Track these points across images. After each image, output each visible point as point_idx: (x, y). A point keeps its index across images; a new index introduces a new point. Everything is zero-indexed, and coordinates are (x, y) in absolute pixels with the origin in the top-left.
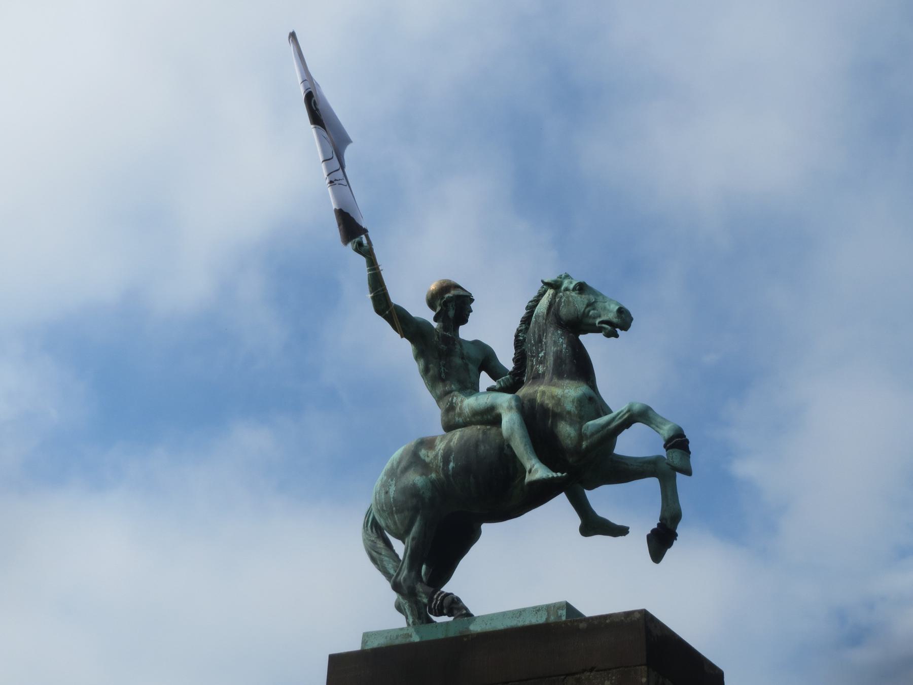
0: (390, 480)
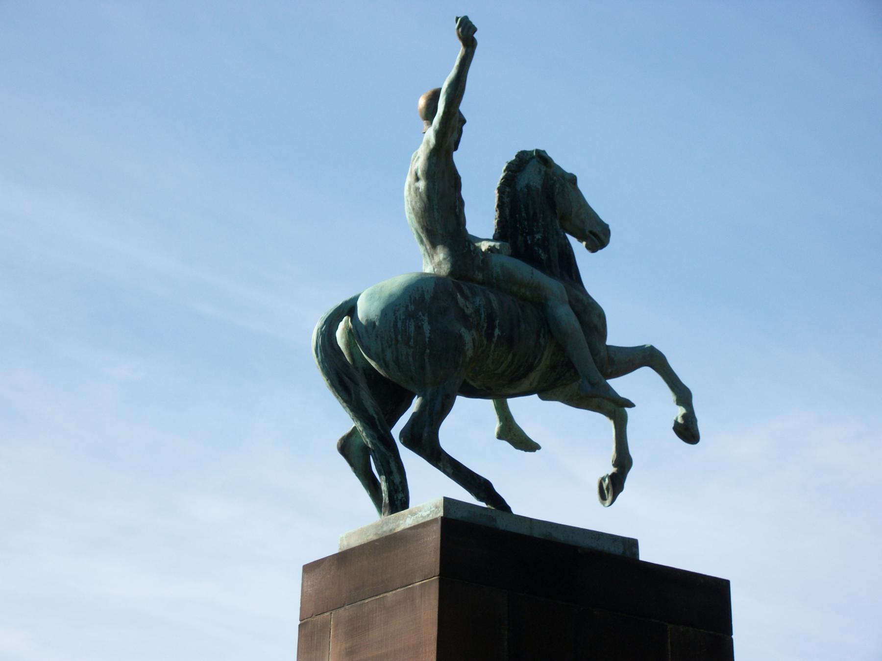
0: (420, 313)
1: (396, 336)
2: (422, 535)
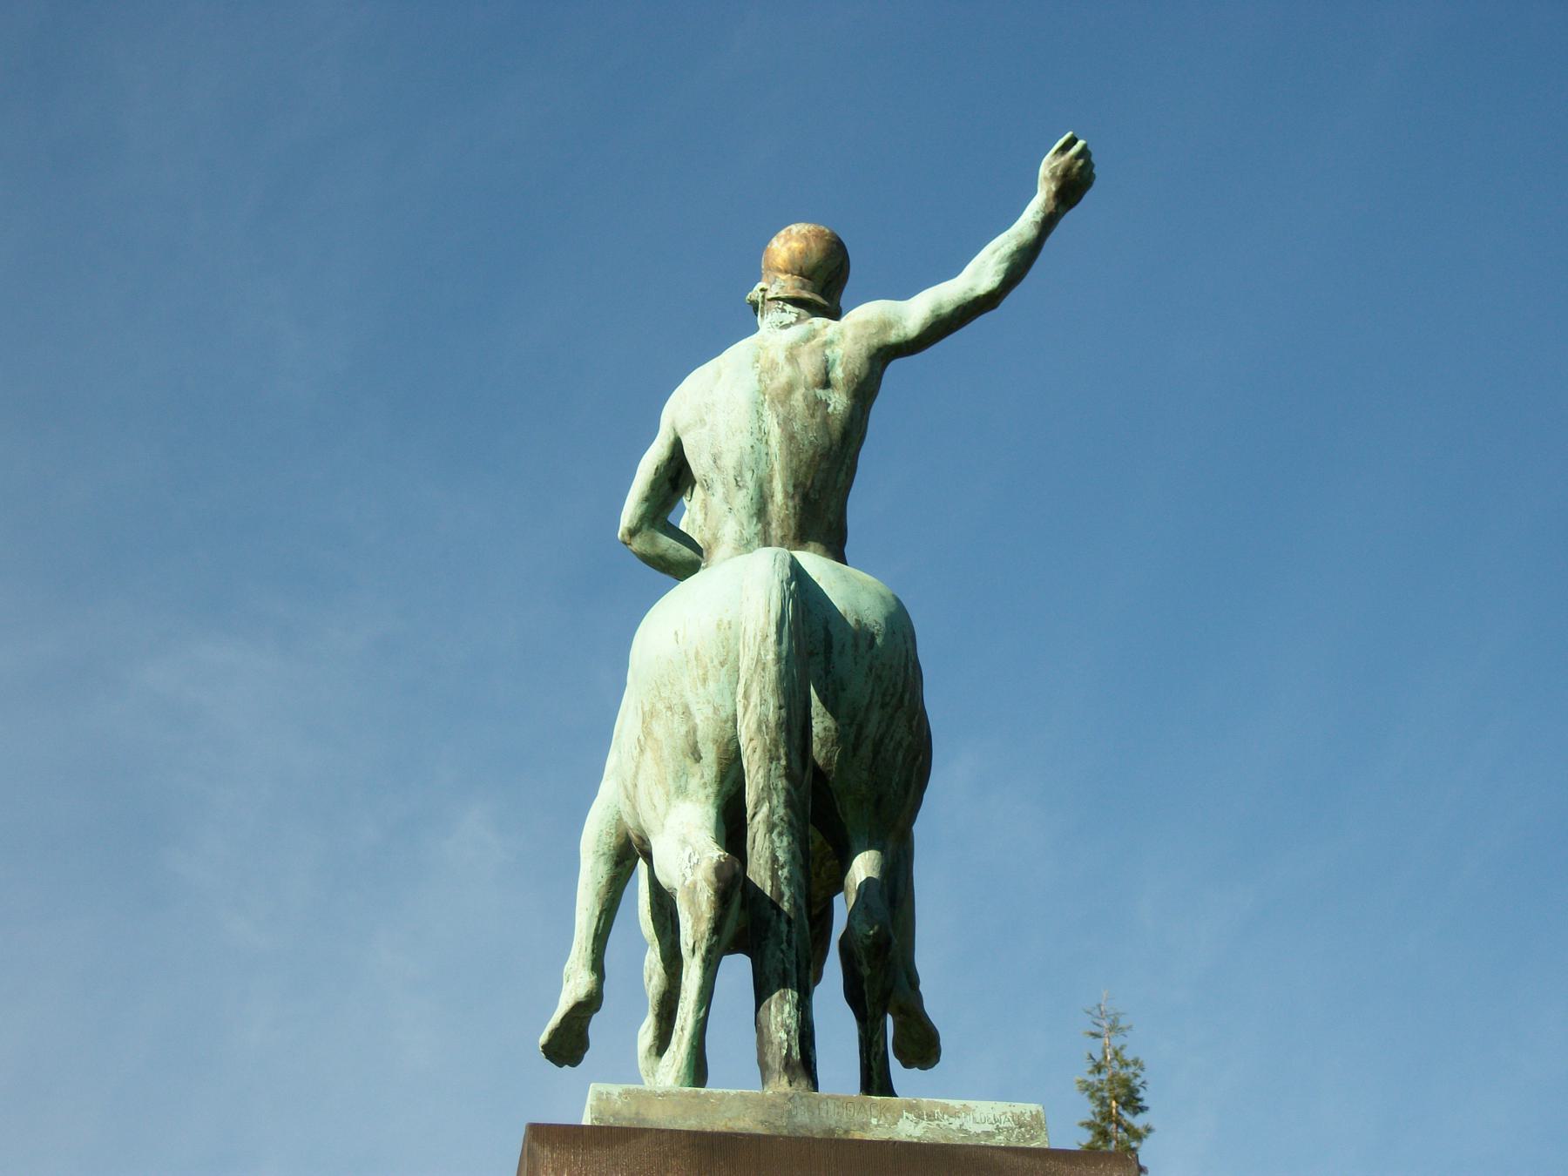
1: (904, 692)
2: (722, 1163)
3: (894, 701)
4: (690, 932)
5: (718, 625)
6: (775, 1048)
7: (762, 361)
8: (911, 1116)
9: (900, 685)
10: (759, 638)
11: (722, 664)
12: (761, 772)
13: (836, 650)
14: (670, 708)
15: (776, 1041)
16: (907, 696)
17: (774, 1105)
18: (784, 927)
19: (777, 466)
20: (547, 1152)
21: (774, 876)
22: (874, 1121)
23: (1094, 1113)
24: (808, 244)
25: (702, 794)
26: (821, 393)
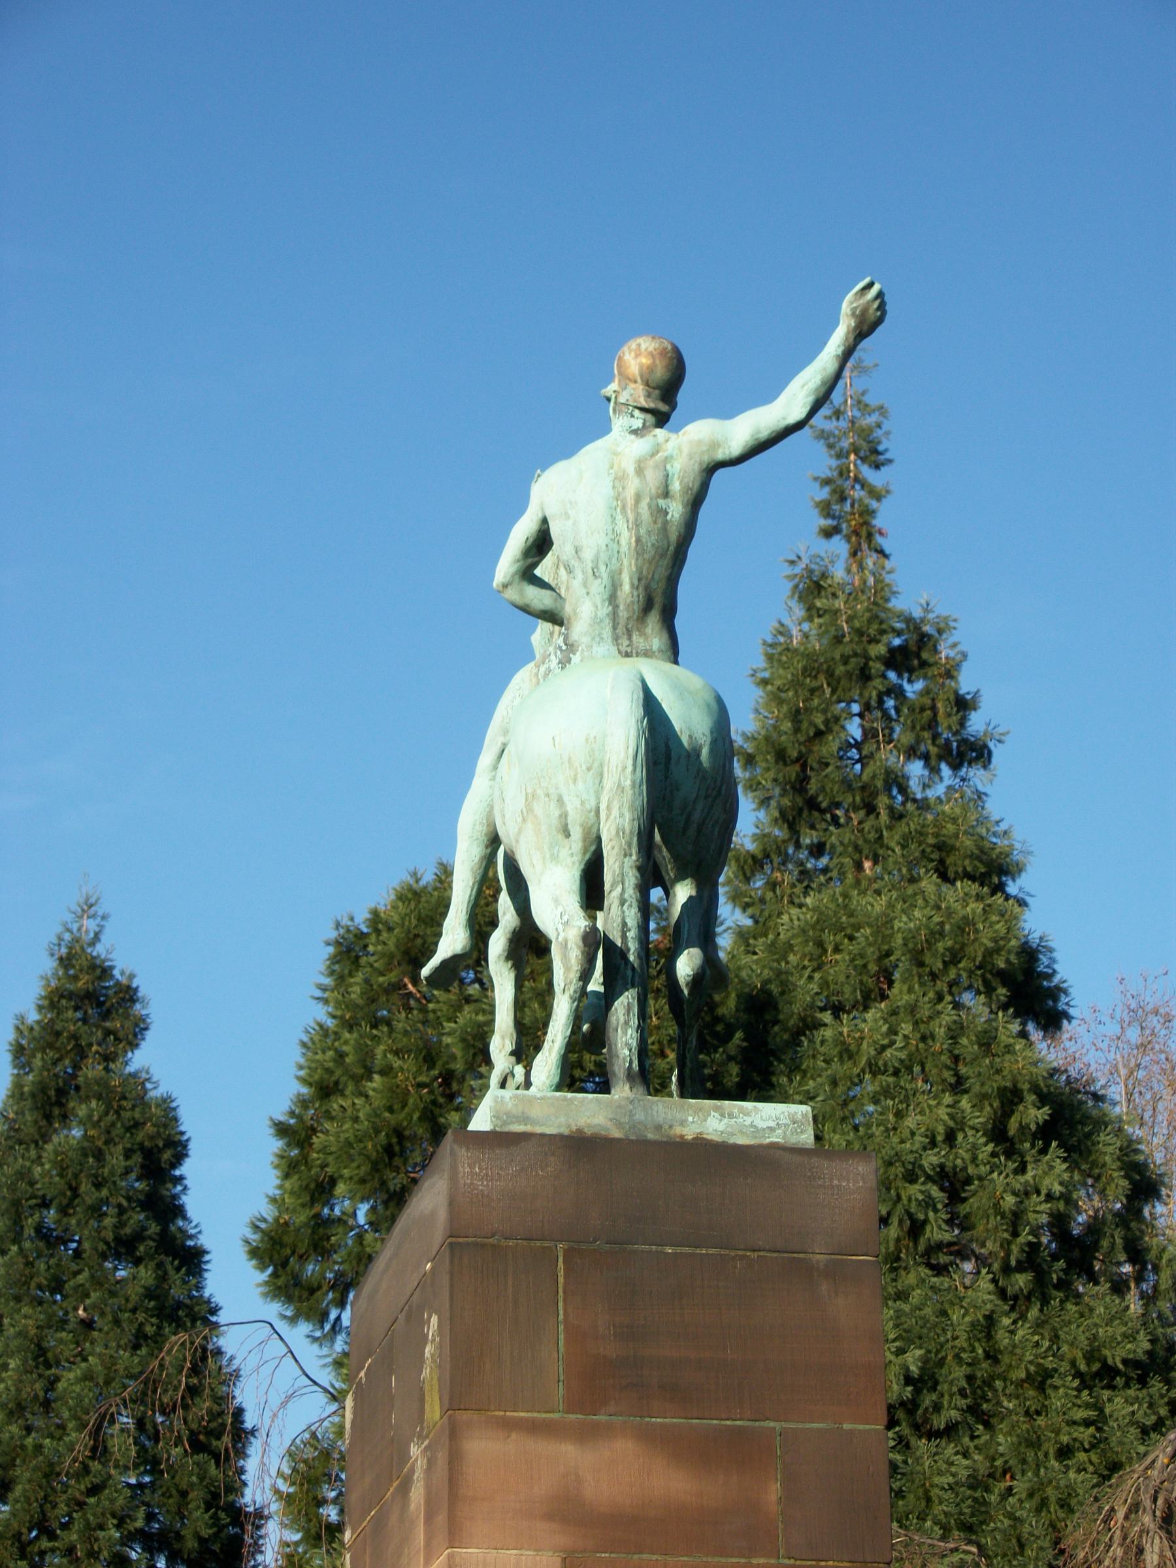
3: (715, 793)
4: (562, 977)
5: (587, 740)
6: (621, 1061)
7: (615, 467)
8: (717, 1115)
9: (719, 779)
10: (620, 768)
11: (589, 769)
12: (617, 864)
13: (673, 762)
14: (547, 795)
15: (621, 1056)
16: (724, 788)
17: (619, 1107)
18: (629, 973)
19: (626, 562)
20: (463, 1151)
21: (624, 937)
22: (690, 1119)
23: (830, 469)
24: (654, 362)
25: (569, 861)
26: (662, 502)
